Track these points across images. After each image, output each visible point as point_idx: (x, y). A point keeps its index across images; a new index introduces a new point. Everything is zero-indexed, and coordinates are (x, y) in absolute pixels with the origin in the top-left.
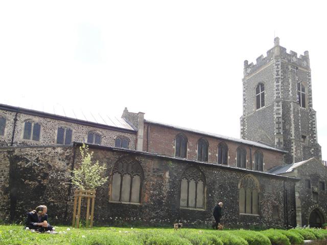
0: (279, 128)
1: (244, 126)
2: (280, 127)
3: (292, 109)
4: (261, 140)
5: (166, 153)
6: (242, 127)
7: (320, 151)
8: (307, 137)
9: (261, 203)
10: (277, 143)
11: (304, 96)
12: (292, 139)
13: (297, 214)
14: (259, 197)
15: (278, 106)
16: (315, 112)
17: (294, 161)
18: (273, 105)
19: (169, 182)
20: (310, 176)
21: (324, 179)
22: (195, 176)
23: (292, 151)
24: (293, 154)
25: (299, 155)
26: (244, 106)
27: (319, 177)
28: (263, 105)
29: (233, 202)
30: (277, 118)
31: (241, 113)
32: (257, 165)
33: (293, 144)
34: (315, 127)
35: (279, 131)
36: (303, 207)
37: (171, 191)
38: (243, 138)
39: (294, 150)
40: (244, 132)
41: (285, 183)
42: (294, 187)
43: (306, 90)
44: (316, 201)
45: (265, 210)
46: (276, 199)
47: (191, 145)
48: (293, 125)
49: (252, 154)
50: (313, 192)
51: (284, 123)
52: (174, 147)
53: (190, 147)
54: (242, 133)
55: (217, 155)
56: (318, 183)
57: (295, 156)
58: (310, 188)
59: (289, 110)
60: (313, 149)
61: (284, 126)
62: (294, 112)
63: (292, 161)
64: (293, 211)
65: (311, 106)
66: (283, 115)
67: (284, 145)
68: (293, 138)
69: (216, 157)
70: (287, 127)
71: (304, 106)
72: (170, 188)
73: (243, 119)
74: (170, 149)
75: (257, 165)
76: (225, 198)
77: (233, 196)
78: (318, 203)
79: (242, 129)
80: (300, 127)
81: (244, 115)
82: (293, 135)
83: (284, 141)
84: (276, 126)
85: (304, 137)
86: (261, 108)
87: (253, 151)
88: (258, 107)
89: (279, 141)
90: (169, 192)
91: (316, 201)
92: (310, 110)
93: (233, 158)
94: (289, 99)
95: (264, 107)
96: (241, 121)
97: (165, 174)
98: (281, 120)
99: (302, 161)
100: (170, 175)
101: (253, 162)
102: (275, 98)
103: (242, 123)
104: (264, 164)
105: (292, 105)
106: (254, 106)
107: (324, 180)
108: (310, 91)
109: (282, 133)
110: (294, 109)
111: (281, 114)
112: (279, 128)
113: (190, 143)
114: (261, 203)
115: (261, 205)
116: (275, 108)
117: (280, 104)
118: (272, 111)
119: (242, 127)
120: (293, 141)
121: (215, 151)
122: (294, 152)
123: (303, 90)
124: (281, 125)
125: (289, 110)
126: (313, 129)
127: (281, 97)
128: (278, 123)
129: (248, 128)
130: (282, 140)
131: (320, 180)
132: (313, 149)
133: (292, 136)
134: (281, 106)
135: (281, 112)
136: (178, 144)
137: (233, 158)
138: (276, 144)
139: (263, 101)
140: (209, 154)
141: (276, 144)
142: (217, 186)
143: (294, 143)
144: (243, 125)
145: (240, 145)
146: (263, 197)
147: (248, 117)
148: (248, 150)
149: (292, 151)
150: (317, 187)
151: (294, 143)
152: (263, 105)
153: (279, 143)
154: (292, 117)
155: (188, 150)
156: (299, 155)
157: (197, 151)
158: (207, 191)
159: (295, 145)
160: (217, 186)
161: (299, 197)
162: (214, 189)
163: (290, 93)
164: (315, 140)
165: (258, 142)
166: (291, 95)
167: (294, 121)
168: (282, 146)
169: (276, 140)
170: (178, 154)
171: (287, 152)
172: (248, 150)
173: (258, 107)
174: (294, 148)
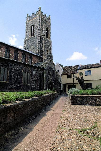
8: (49, 51)
11: (48, 33)
15: (39, 36)
17: (44, 61)
18: (37, 36)
24: (43, 58)
28: (33, 35)
34: (51, 47)
38: (25, 49)
39: (44, 56)
40: (25, 46)
43: (49, 31)
48: (44, 45)
54: (24, 47)
55: (14, 56)
61: (41, 45)
65: (50, 38)
66: (41, 41)
70: (42, 46)
71: (48, 38)
73: (25, 40)
76: (17, 76)
77: (20, 76)
82: (44, 50)
85: (47, 51)
86: (32, 36)
87: (29, 55)
88: (31, 36)
93: (20, 58)
96: (24, 41)
98: (40, 42)
101: (29, 60)
102: (38, 32)
104: (33, 61)
105: (44, 37)
106: (30, 35)
116: (38, 37)
117: (40, 35)
123: (48, 31)
124: (40, 45)
125: (43, 39)
130: (40, 52)
135: (40, 39)
137: (20, 58)
139: (33, 34)
140: (10, 55)
141: (37, 53)
144: (25, 43)
148: (27, 55)
152: (33, 35)
153: (39, 52)
154: (44, 42)
157: (5, 53)
161: (45, 76)
163: (43, 32)
166: (44, 32)
168: (40, 54)
169: (38, 51)
173: (31, 36)
174: (44, 55)
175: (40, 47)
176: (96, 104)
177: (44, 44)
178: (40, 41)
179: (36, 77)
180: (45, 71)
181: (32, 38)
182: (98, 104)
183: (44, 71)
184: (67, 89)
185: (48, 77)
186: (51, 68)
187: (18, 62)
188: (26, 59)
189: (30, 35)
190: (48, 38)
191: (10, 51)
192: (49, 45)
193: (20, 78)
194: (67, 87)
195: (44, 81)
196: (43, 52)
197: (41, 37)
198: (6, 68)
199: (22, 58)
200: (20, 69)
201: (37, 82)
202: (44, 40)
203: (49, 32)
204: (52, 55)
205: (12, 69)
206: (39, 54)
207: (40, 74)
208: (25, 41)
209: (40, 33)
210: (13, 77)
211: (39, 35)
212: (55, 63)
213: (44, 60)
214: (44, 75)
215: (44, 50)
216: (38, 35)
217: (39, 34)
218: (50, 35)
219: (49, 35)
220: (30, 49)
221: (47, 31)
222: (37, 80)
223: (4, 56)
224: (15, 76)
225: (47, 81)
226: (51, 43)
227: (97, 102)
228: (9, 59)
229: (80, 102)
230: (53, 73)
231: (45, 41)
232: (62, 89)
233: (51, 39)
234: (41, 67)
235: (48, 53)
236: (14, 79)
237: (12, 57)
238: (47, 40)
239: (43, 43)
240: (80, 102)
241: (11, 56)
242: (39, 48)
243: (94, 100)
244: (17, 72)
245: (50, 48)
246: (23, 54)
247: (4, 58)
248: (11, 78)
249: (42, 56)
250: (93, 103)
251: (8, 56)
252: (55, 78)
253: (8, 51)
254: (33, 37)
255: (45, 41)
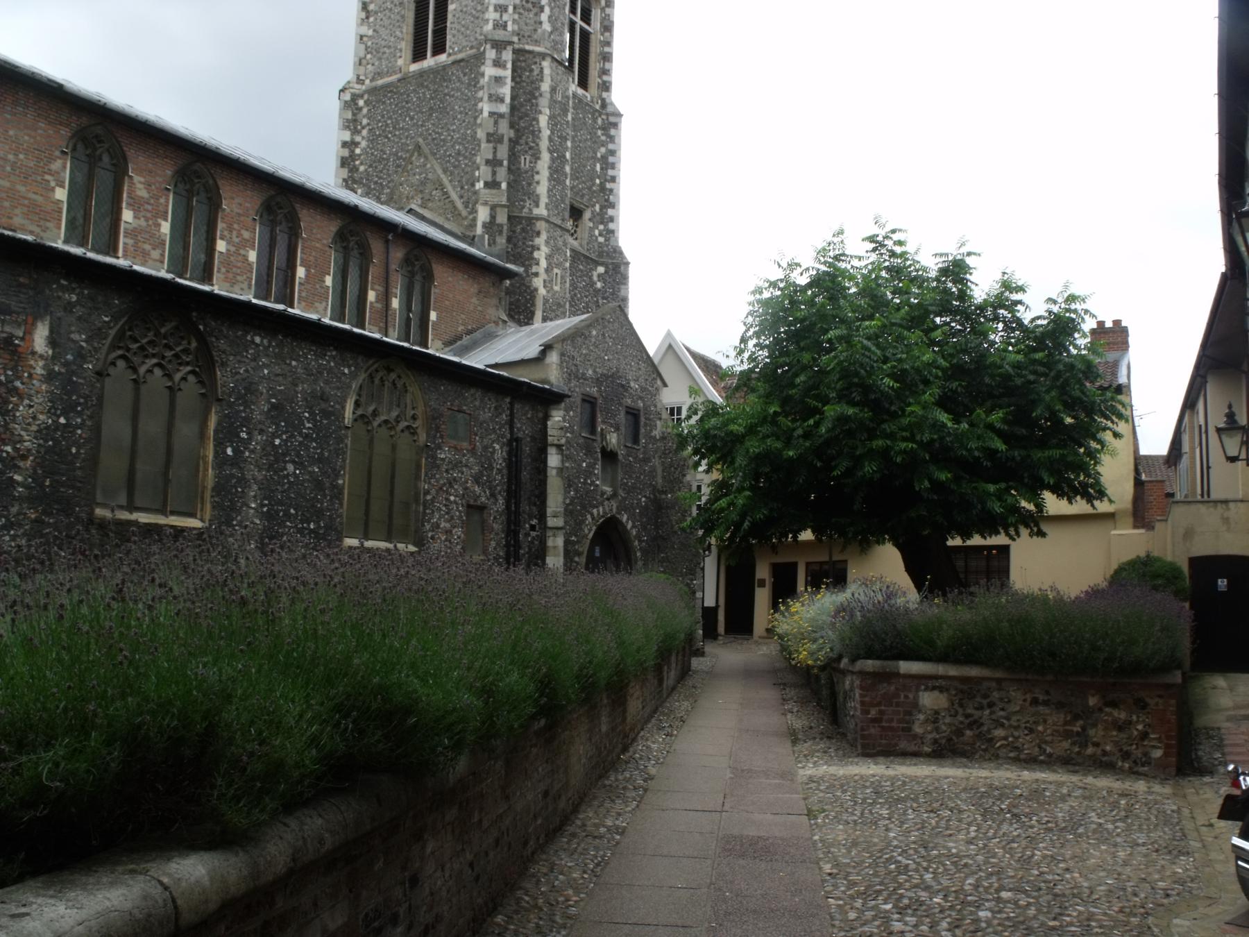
0: (493, 163)
1: (356, 132)
2: (499, 156)
3: (545, 86)
4: (423, 206)
5: (17, 221)
6: (347, 136)
7: (624, 279)
8: (587, 215)
9: (427, 492)
10: (485, 225)
11: (585, 36)
12: (538, 218)
13: (550, 543)
14: (418, 467)
15: (498, 63)
16: (619, 115)
17: (539, 315)
18: (479, 58)
19: (50, 377)
20: (598, 381)
21: (641, 398)
22: (169, 354)
23: (534, 269)
24: (538, 283)
25: (557, 288)
26: (362, 37)
27: (625, 388)
28: (439, 48)
29: (319, 485)
30: (491, 114)
31: (347, 73)
32: (408, 320)
33: (541, 241)
34: (613, 179)
35: (494, 173)
36: (569, 512)
37: (57, 426)
38: (349, 184)
39: (543, 263)
40: (353, 157)
41: (517, 406)
42: (546, 427)
43: (596, 15)
44: (608, 489)
45: (438, 526)
46: (480, 474)
47: (142, 192)
48: (545, 157)
49: (393, 267)
50: (603, 450)
51: (514, 143)
52: (61, 194)
53: (136, 206)
54: (344, 162)
55: (252, 256)
56: (623, 414)
57: (542, 291)
58: (593, 430)
59: (538, 88)
60: (601, 269)
61: (513, 157)
62: (553, 102)
63: (533, 314)
64: (533, 528)
65: (606, 87)
66: (513, 108)
67: (509, 240)
68: (541, 211)
69: (250, 265)
70: (525, 162)
71: (583, 83)
72: (51, 412)
73: (355, 98)
74: (39, 199)
75: (408, 320)
76: (290, 467)
77: (321, 460)
78: (614, 495)
79: (345, 144)
80: (568, 169)
81: (360, 81)
82: (544, 200)
83: (510, 218)
84: (486, 150)
85: (576, 213)
86: (430, 62)
87: (398, 254)
88: (419, 54)
89: (493, 217)
90: (44, 433)
91: (608, 489)
92: (604, 105)
93: (315, 278)
94: (537, 42)
95: (443, 58)
96: (347, 105)
97: (29, 333)
98: (504, 128)
99: (563, 315)
100: (52, 341)
101: (395, 303)
102: (490, 26)
103: (610, 212)
104: (433, 316)
105: (547, 71)
106: (406, 47)
107: (641, 404)
108: (608, 27)
109: (504, 185)
110: (553, 90)
111: (508, 100)
112: (493, 163)
113: (138, 184)
114: (427, 492)
115: (425, 502)
116: (489, 71)
117: (508, 56)
118: (474, 84)
119: (347, 136)
120: (541, 225)
121: (246, 235)
122: (543, 276)
123: (586, 17)
124: (503, 152)
125: (533, 94)
126: (608, 186)
127: (510, 28)
128: (494, 138)
129: (372, 140)
130: (502, 218)
131: (629, 401)
132: (601, 269)
133: (537, 206)
134: (509, 65)
135: (506, 91)
136: (80, 178)
137: (315, 278)
138: (479, 230)
139: (440, 34)
140: (221, 246)
141: (479, 230)
142: (259, 410)
143: (544, 236)
144: (352, 125)
145: (85, 120)
146: (434, 464)
147: (373, 91)
148: (376, 246)
149: (534, 269)
150: (617, 429)
151: (544, 236)
152: (439, 48)
153: (490, 226)
154: (543, 120)
155: (127, 215)
156: (557, 288)
157: (166, 227)
158: (216, 431)
159: (547, 242)
160: (259, 410)
161: (560, 470)
162: (247, 420)
163: (544, 17)
164: (610, 234)
165: (410, 211)
166: (547, 27)
167: (550, 139)
168: (502, 241)
169: (483, 214)
170: (77, 232)
171: (521, 270)
172: (376, 246)
173: (419, 54)
174: (541, 255)
175: (502, 173)
176: (1090, 750)
177: (544, 144)
178: (504, 108)
179: (477, 480)
180: (557, 417)
181: (421, 74)
182: (1105, 753)
183: (547, 417)
184: (762, 597)
185: (589, 473)
186: (613, 383)
187: (211, 295)
188: (372, 296)
189: (403, 45)
190: (583, 83)
191: (214, 205)
192: (594, 158)
193: (319, 485)
194: (762, 583)
195: (551, 522)
196: (531, 220)
197: (523, 65)
198: (191, 378)
199: (329, 281)
200: (324, 398)
201: (483, 525)
202: (544, 103)
203: (595, 27)
204: (618, 252)
205: (248, 391)
206: (492, 243)
207: (514, 446)
208: (351, 105)
209: (505, 27)
210: (253, 472)
211: (499, 45)
212: (652, 345)
213: (539, 304)
214: (553, 460)
215: (544, 200)
216: (491, 54)
217: (500, 35)
218: (607, 58)
219: (593, 57)
220: (405, 190)
221: (573, 10)
222: (482, 508)
223: (155, 254)
224: (275, 459)
225: (573, 513)
226: (612, 139)
227: (1095, 733)
228: (206, 288)
229: (937, 730)
230: (636, 440)
231: (559, 109)
232: (710, 602)
233: (619, 97)
234: (524, 376)
235: (583, 232)
236: (267, 490)
237: (234, 263)
238: (579, 102)
239: (536, 134)
240: (937, 730)
241: (227, 263)
242: (492, 184)
243: (1076, 717)
244: (294, 425)
245: (602, 188)
246: (341, 238)
247: (248, 304)
248: (243, 481)
249: (526, 258)
250: (1066, 744)
251: (195, 255)
252: (654, 489)
253: (104, 177)
254: (434, 71)
255: (551, 117)
